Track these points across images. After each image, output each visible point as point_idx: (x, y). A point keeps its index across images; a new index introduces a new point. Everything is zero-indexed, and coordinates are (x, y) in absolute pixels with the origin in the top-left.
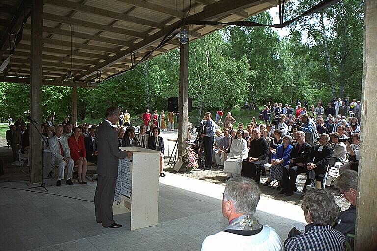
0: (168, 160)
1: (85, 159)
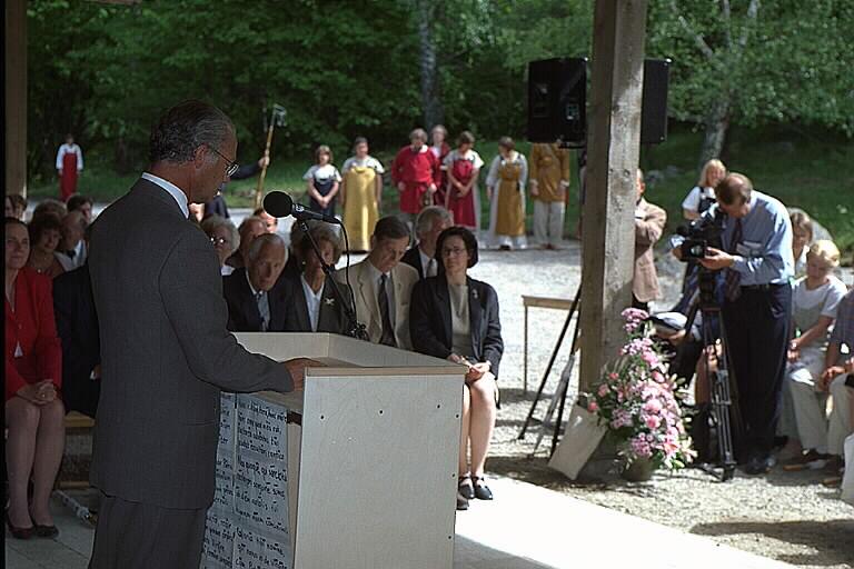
0: (521, 411)
1: (52, 396)
